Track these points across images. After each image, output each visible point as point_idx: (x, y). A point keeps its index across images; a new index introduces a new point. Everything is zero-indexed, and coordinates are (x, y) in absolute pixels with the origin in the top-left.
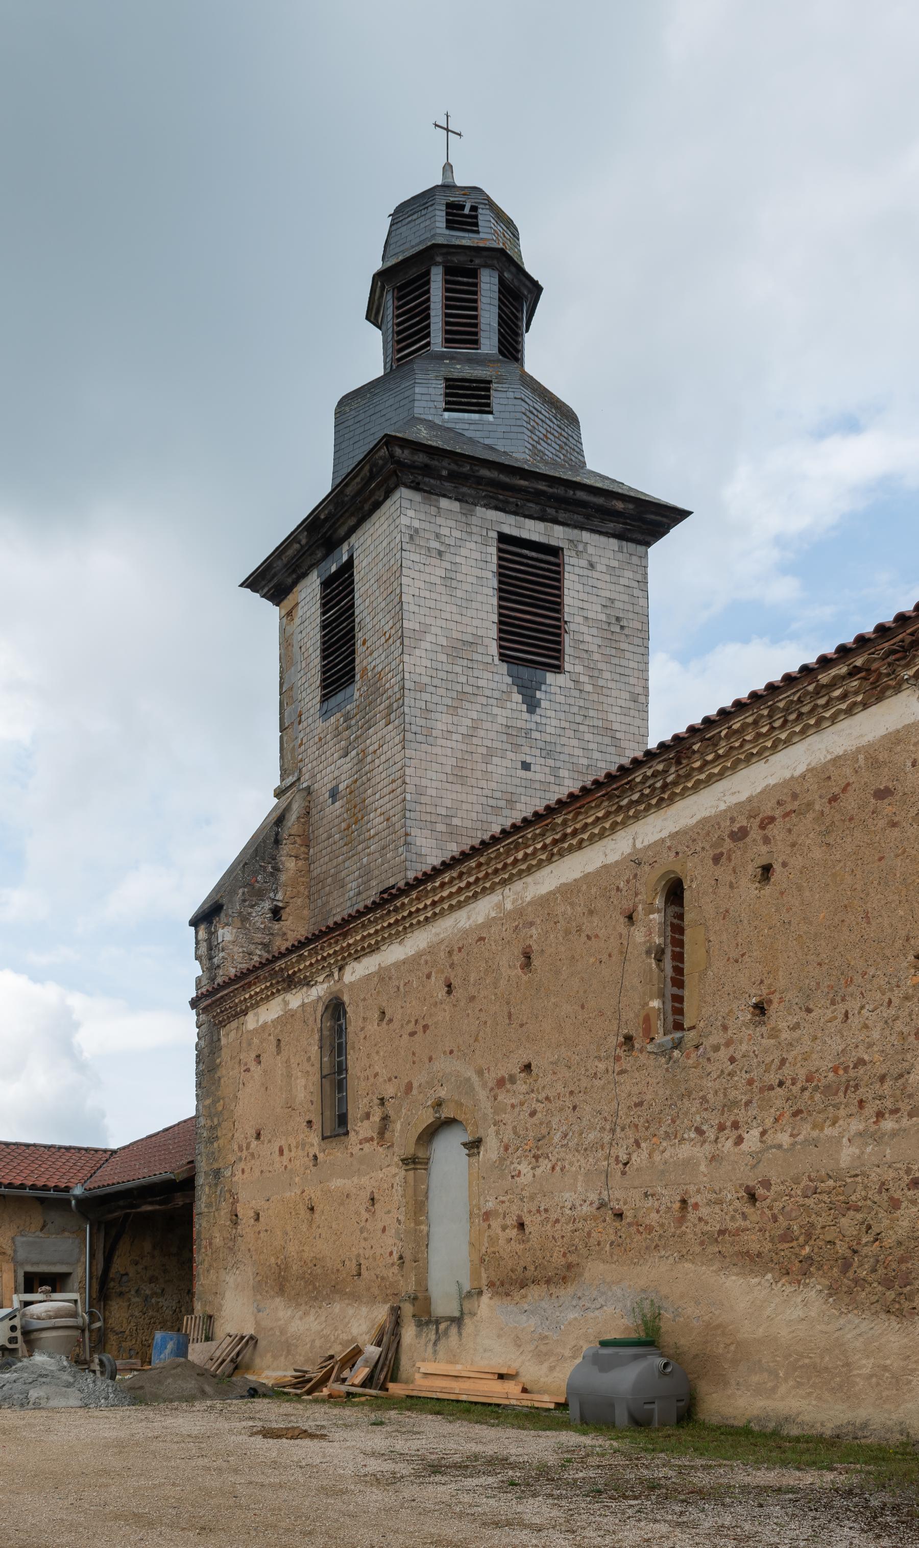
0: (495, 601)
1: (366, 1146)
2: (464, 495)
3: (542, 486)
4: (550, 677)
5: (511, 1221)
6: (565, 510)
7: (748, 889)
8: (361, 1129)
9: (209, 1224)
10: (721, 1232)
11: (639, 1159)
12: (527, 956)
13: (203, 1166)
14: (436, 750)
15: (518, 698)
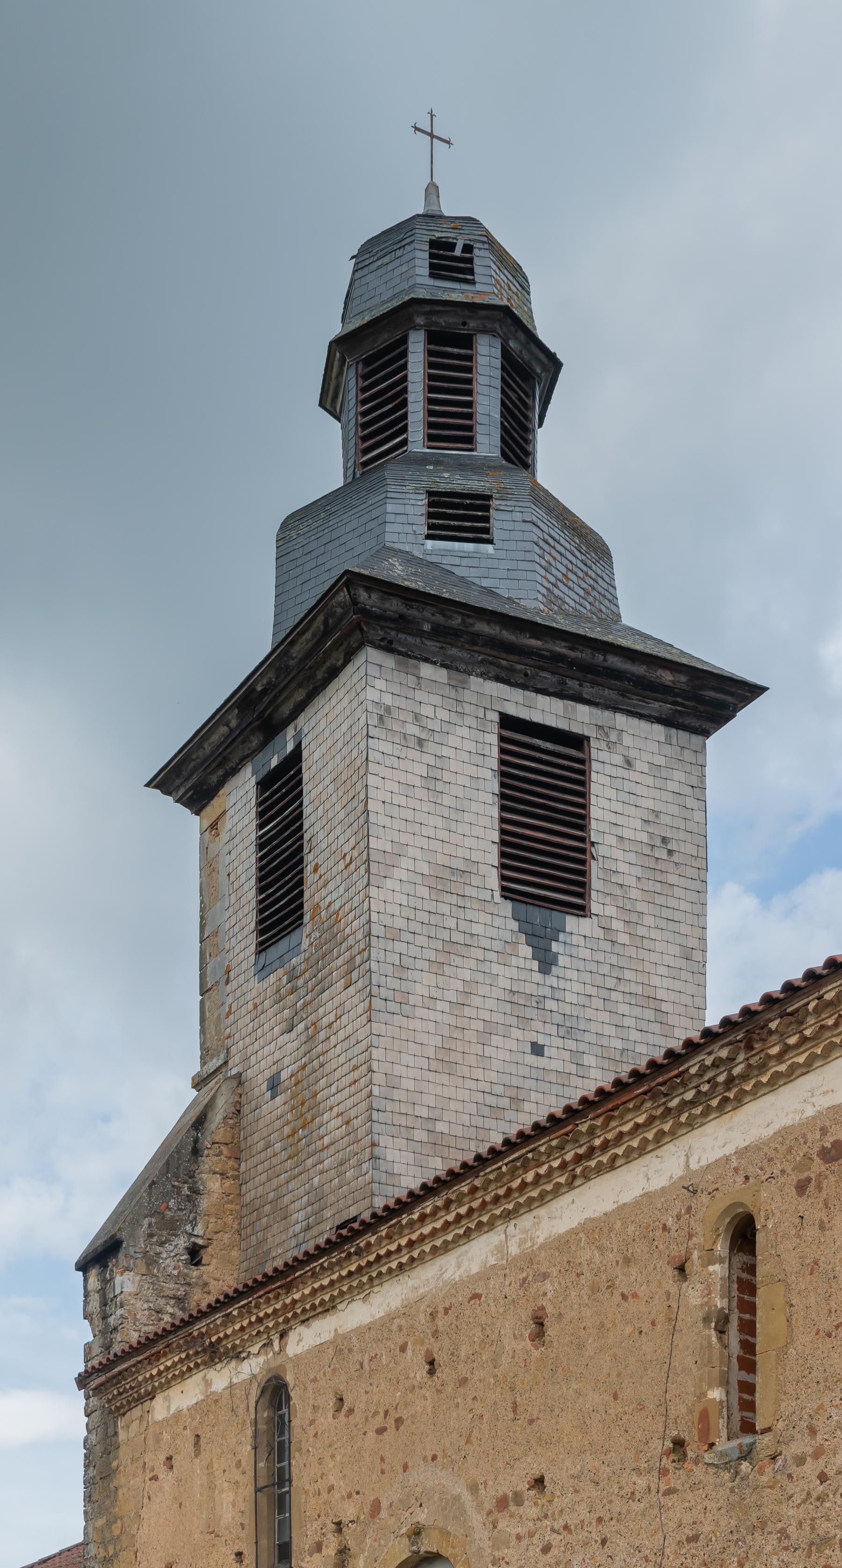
0: (495, 812)
2: (453, 659)
3: (560, 648)
4: (571, 922)
6: (594, 683)
14: (416, 1024)
15: (527, 951)
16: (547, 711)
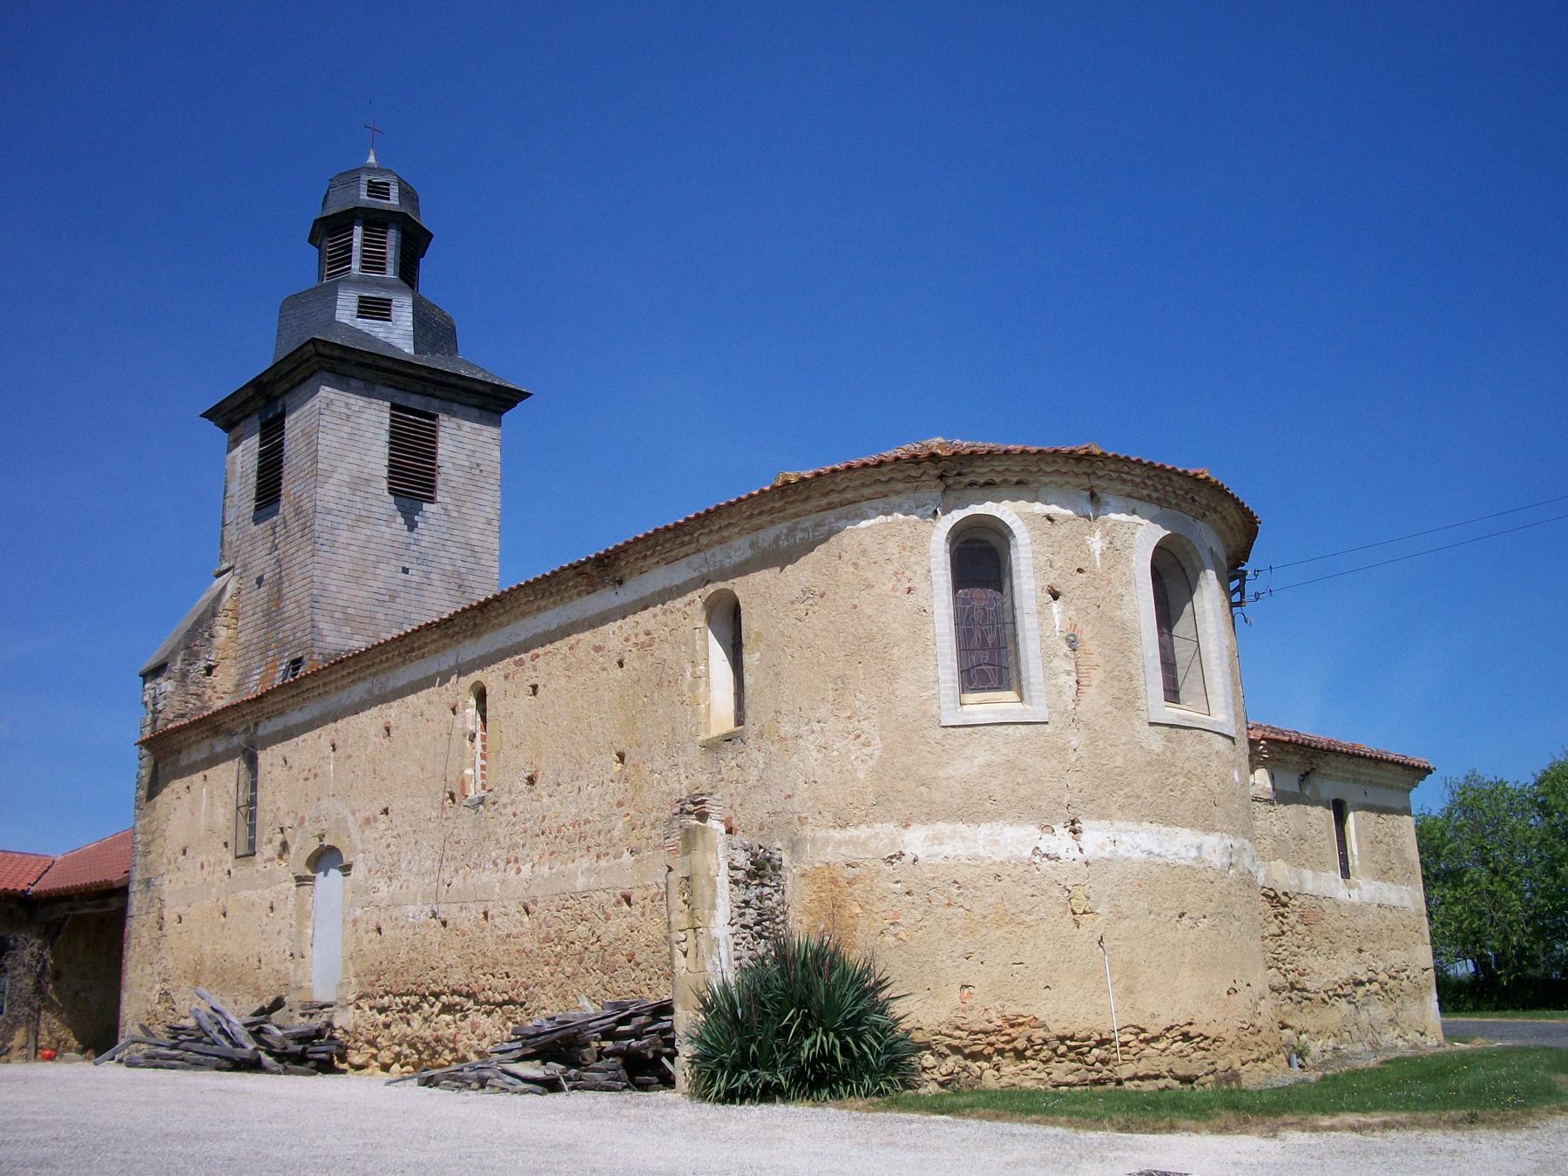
0: (387, 451)
1: (269, 865)
4: (425, 506)
5: (372, 927)
7: (526, 700)
8: (267, 851)
9: (139, 927)
10: (508, 936)
11: (457, 882)
12: (388, 729)
13: (137, 875)
14: (340, 558)
15: (401, 520)
16: (416, 402)
